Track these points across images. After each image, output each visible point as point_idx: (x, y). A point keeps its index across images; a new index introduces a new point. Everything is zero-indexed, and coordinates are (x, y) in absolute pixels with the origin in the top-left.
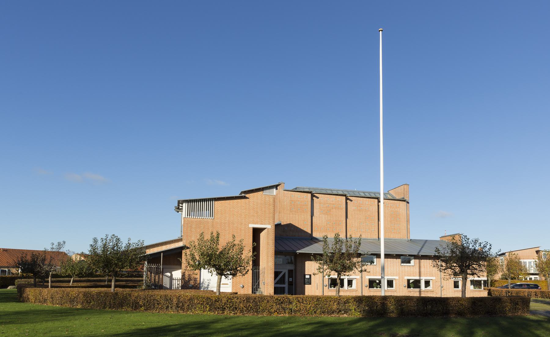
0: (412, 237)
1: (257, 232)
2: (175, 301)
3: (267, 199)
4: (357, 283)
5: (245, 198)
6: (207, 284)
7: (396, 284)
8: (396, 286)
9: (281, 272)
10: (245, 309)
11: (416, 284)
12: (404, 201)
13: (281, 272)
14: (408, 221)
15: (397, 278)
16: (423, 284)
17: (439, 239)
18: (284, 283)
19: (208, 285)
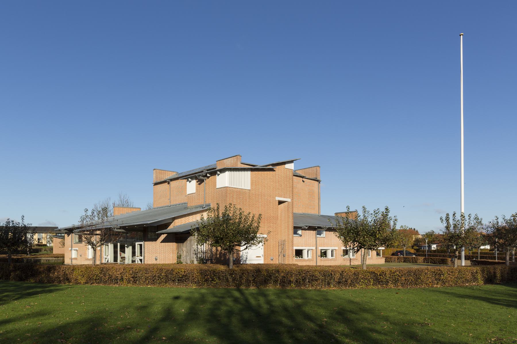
0: (322, 213)
1: (448, 215)
2: (338, 275)
3: (288, 173)
4: (313, 254)
5: (272, 170)
6: (245, 257)
7: (336, 254)
8: (336, 255)
9: (162, 242)
10: (210, 279)
11: (324, 254)
12: (317, 181)
13: (162, 242)
14: (319, 199)
15: (337, 248)
16: (329, 253)
17: (334, 215)
18: (406, 255)
19: (247, 258)
